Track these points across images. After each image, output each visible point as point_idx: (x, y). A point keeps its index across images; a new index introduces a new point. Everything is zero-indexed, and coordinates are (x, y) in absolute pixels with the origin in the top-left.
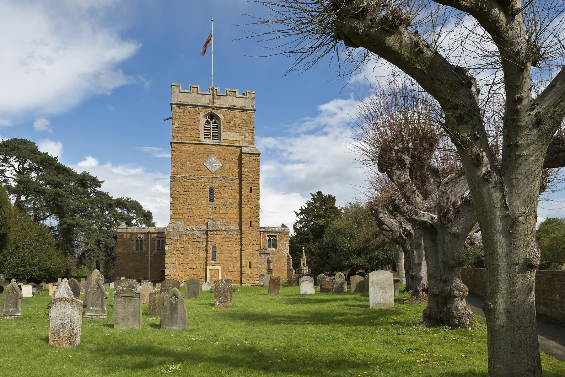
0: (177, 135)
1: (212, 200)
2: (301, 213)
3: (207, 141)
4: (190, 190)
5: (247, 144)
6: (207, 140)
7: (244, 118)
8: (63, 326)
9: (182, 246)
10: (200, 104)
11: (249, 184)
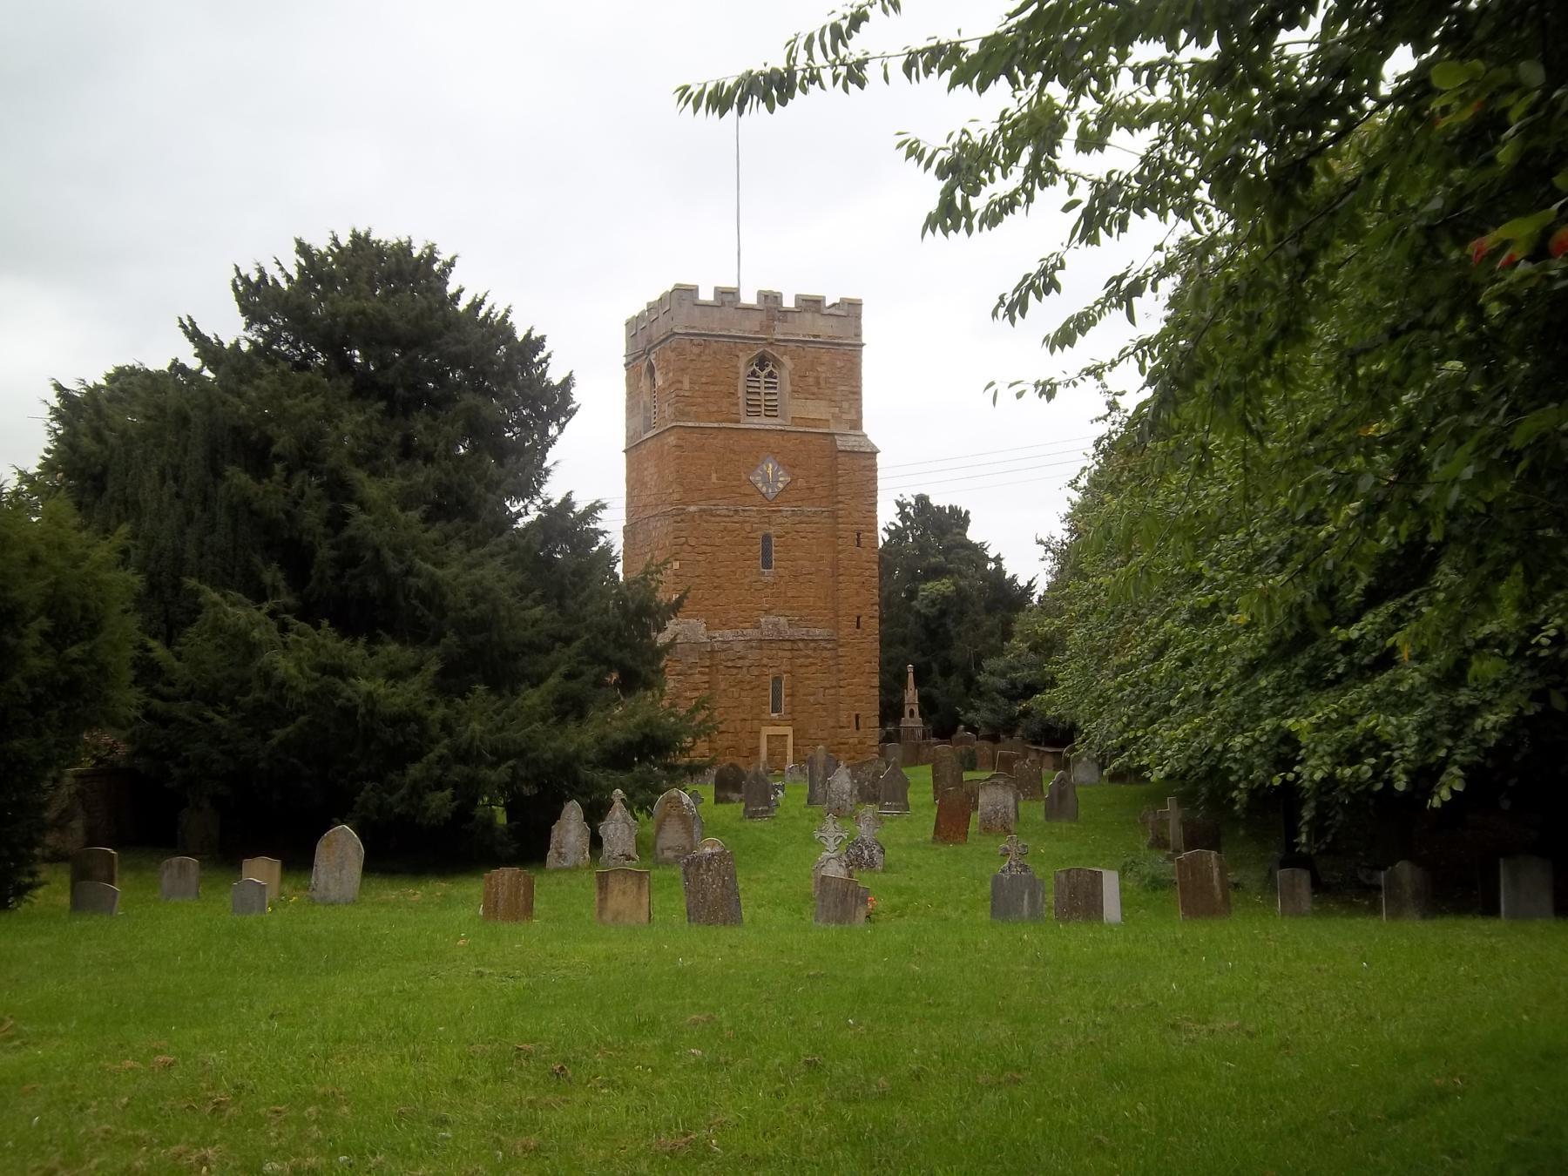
1: (767, 564)
4: (717, 542)
6: (756, 420)
7: (839, 364)
9: (706, 678)
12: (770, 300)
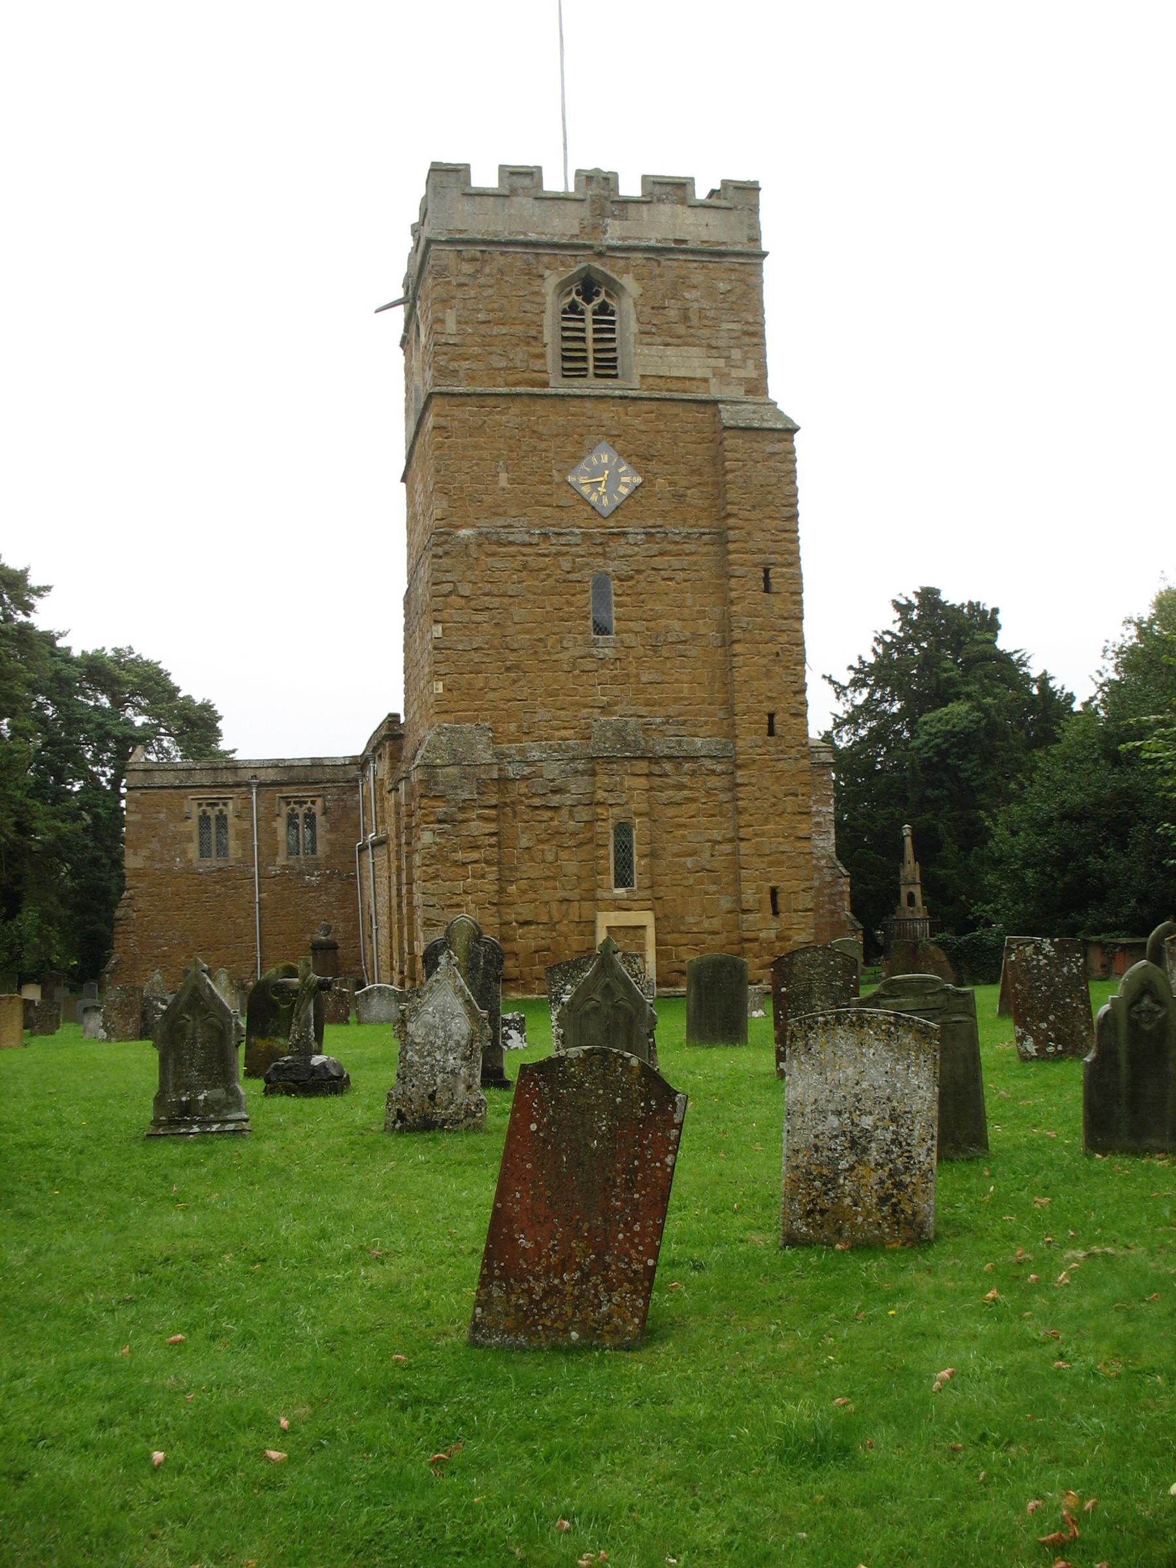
0: (454, 365)
2: (856, 684)
3: (578, 386)
4: (511, 589)
5: (738, 392)
6: (577, 382)
7: (722, 286)
8: (854, 1143)
9: (491, 827)
10: (544, 238)
11: (759, 558)
12: (597, 185)
